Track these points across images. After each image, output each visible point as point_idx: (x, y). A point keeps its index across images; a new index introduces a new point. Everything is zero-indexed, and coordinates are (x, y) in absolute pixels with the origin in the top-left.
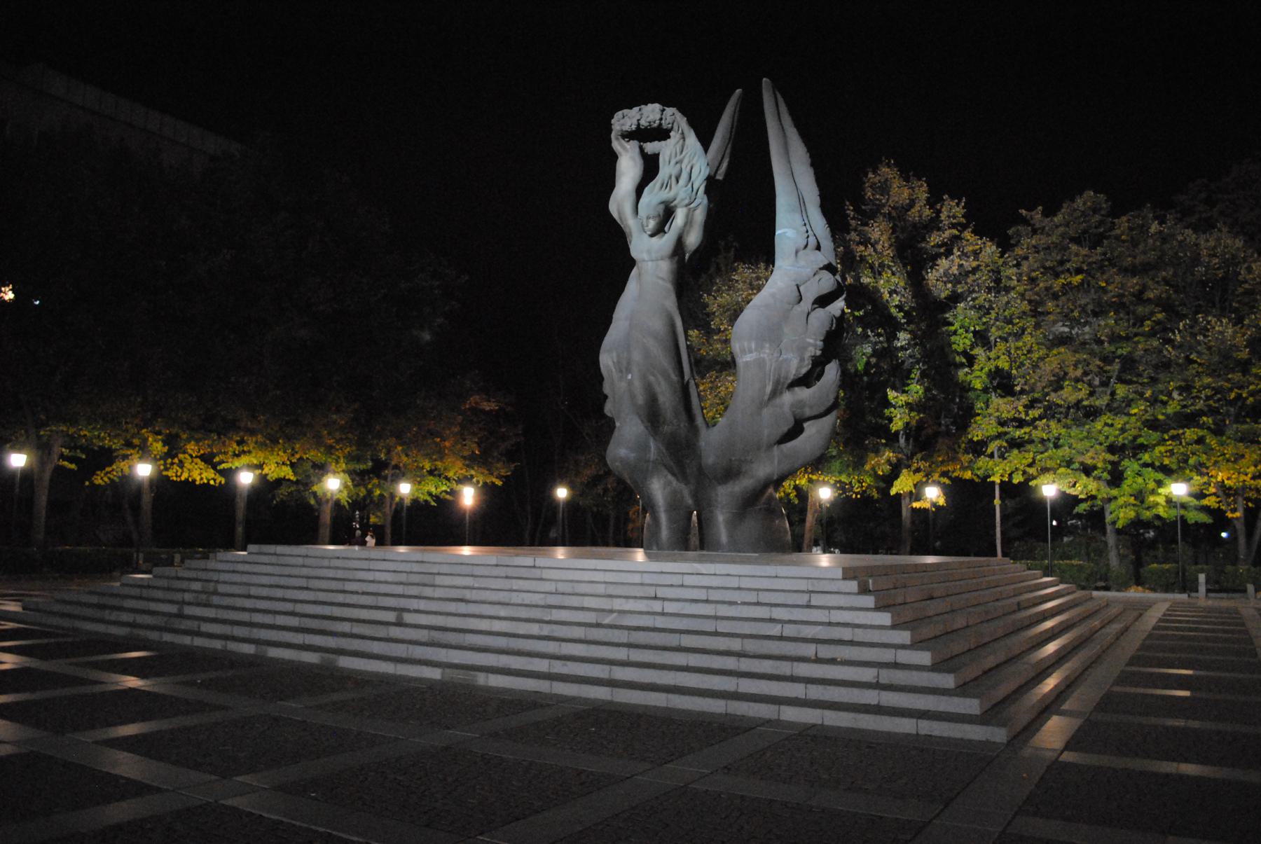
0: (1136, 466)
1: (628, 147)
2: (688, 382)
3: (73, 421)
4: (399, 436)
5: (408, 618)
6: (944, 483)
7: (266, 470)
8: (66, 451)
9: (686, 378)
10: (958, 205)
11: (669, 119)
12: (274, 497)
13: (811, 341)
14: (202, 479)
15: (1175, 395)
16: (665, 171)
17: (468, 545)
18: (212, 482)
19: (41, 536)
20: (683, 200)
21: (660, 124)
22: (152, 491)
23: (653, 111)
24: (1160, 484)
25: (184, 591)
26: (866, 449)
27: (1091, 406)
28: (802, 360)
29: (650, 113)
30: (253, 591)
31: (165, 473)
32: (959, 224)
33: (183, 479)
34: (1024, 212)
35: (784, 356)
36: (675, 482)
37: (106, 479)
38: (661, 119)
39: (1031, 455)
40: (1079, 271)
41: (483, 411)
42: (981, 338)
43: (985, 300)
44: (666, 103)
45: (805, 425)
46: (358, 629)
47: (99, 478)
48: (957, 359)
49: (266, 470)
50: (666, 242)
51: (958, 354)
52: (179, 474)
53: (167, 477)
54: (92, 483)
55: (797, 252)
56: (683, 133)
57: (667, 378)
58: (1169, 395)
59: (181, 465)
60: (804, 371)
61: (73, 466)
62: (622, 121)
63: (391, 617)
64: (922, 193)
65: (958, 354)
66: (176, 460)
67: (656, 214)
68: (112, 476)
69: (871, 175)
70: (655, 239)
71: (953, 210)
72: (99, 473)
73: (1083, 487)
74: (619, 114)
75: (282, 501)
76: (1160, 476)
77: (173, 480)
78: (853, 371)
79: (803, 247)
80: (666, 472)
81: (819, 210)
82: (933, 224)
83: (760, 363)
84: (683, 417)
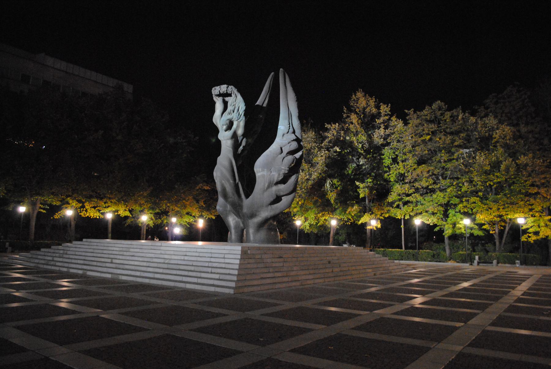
0: (454, 212)
1: (219, 99)
2: (238, 183)
3: (43, 196)
4: (168, 200)
5: (114, 261)
6: (381, 219)
7: (119, 213)
8: (42, 206)
9: (237, 182)
10: (387, 107)
11: (230, 90)
12: (125, 223)
13: (283, 168)
14: (94, 216)
15: (465, 184)
16: (230, 108)
17: (201, 241)
18: (98, 217)
19: (33, 237)
20: (235, 119)
21: (227, 92)
22: (75, 220)
23: (224, 87)
24: (462, 219)
25: (57, 253)
26: (348, 205)
27: (432, 188)
28: (279, 174)
29: (223, 88)
30: (77, 253)
31: (80, 214)
32: (388, 114)
33: (86, 216)
34: (406, 111)
35: (272, 173)
36: (237, 219)
37: (59, 216)
38: (227, 90)
39: (411, 208)
40: (428, 134)
41: (204, 189)
42: (395, 160)
43: (396, 145)
44: (229, 84)
45: (283, 198)
46: (99, 264)
47: (56, 216)
48: (385, 169)
49: (119, 213)
50: (230, 133)
51: (386, 167)
52: (85, 214)
53: (81, 215)
54: (54, 218)
55: (283, 135)
56: (236, 95)
57: (228, 181)
58: (463, 184)
59: (86, 211)
60: (280, 178)
61: (44, 211)
62: (215, 91)
63: (109, 260)
64: (372, 102)
65: (386, 167)
66: (85, 209)
67: (226, 123)
68: (61, 215)
69: (353, 96)
70: (227, 132)
71: (385, 109)
72: (56, 214)
73: (431, 221)
74: (214, 88)
75: (129, 224)
76: (462, 216)
77: (83, 217)
78: (347, 173)
79: (286, 132)
80: (233, 215)
81: (298, 118)
82: (379, 115)
83: (263, 176)
84: (236, 195)
